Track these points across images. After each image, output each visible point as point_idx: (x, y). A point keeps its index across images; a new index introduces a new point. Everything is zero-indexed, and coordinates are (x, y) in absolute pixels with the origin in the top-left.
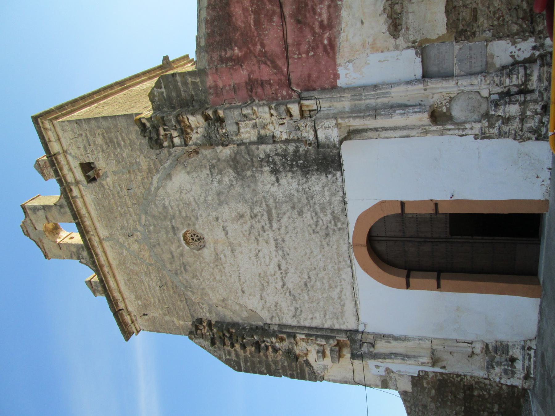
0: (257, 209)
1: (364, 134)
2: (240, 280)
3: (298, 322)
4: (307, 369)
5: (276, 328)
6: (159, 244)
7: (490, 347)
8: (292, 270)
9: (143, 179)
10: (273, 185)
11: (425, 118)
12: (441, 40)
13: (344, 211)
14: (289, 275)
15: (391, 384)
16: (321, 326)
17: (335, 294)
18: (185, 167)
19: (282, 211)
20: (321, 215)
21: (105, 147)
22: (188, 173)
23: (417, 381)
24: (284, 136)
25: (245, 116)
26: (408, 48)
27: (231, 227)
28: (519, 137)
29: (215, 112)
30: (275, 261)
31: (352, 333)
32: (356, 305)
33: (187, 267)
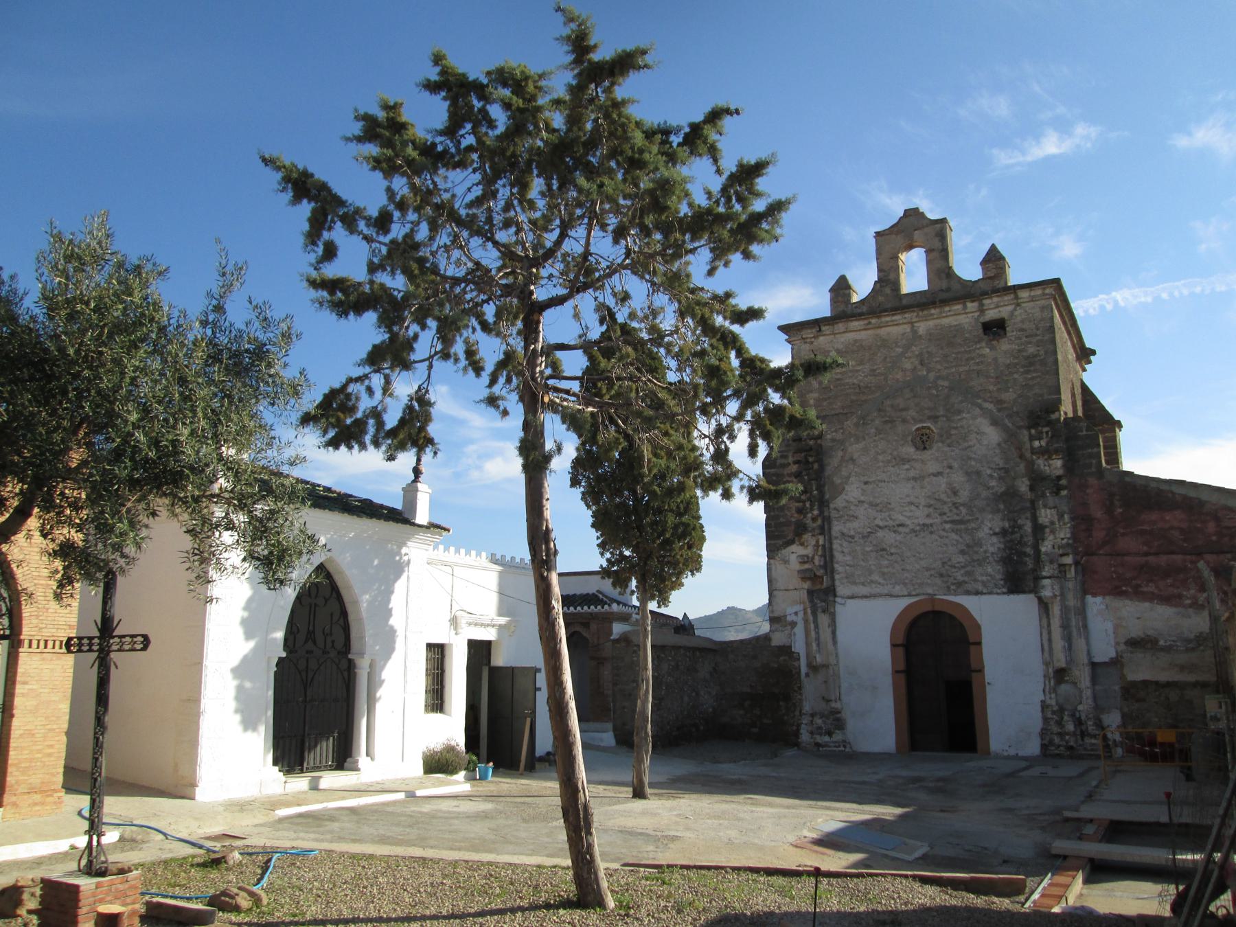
0: (964, 510)
1: (1045, 616)
2: (881, 481)
3: (837, 538)
4: (780, 542)
5: (826, 514)
6: (915, 397)
7: (838, 716)
8: (899, 538)
9: (990, 392)
10: (991, 529)
11: (1062, 664)
12: (1123, 677)
13: (968, 593)
14: (893, 535)
15: (776, 626)
16: (835, 560)
17: (876, 577)
18: (1006, 442)
19: (964, 535)
20: (962, 571)
21: (1025, 354)
22: (999, 445)
23: (786, 650)
24: (1043, 549)
25: (1063, 516)
26: (1117, 652)
27: (942, 481)
28: (1043, 733)
29: (1064, 488)
30: (908, 522)
31: (831, 591)
32: (866, 597)
33: (890, 425)
